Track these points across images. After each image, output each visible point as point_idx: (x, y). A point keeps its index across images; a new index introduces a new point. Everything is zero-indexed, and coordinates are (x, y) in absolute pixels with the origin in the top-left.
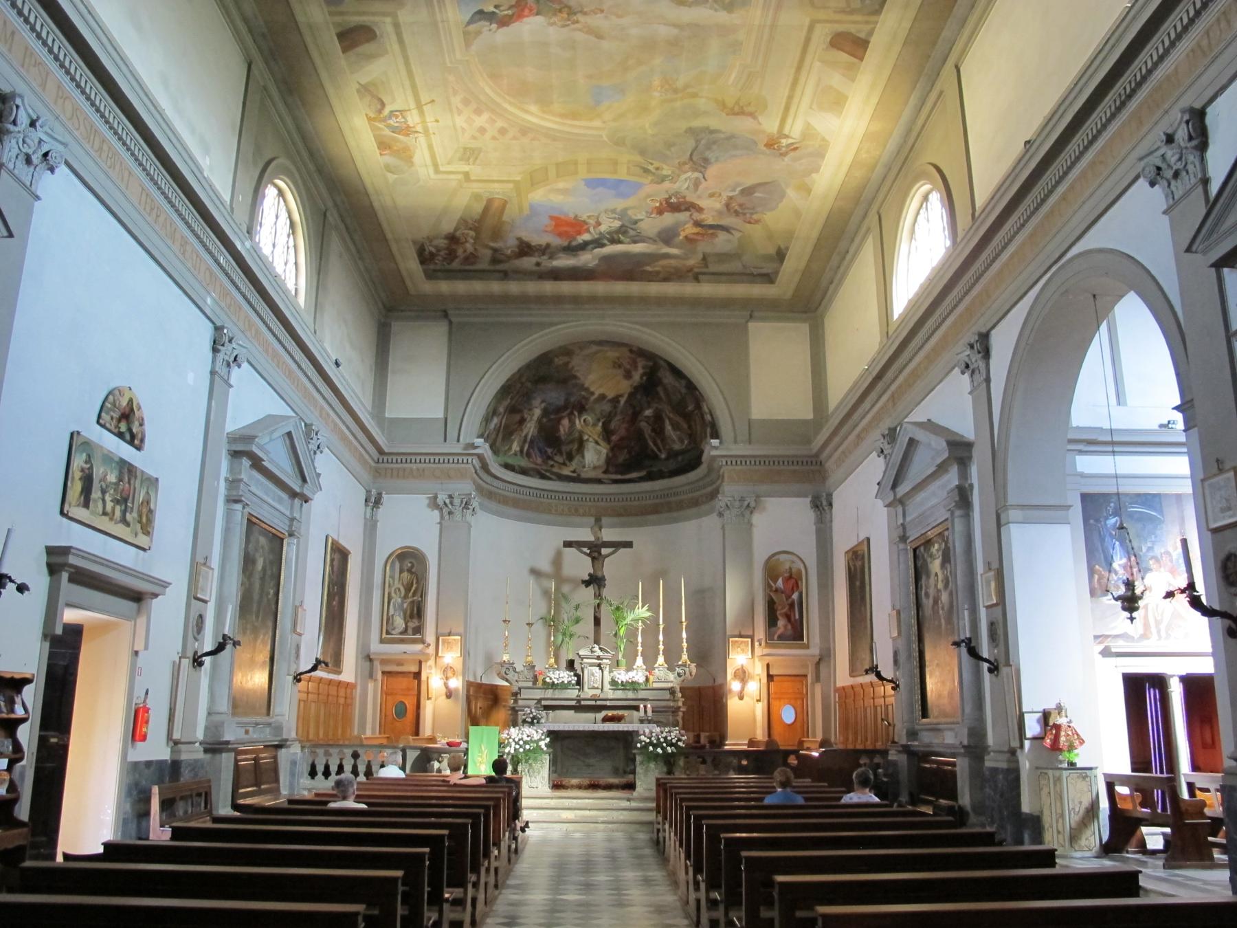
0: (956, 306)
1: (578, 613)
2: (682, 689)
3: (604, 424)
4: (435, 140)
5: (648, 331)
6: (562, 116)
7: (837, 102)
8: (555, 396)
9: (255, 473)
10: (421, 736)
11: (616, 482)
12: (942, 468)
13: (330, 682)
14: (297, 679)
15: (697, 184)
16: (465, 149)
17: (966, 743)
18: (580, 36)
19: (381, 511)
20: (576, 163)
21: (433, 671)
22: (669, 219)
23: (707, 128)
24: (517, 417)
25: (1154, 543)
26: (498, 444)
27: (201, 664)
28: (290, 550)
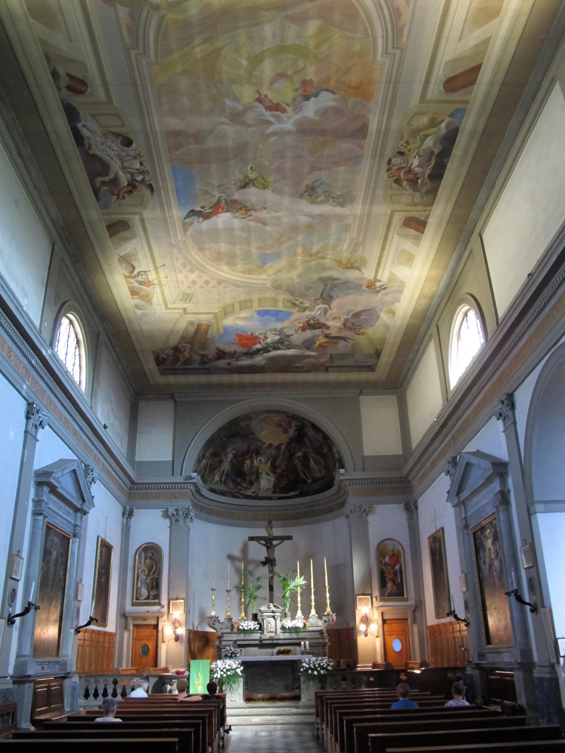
0: (491, 378)
1: (259, 583)
2: (328, 631)
3: (271, 462)
4: (166, 289)
6: (243, 272)
7: (409, 259)
8: (241, 445)
10: (158, 668)
11: (280, 498)
12: (489, 480)
13: (99, 632)
14: (78, 631)
15: (325, 311)
16: (184, 294)
17: (519, 661)
18: (252, 224)
19: (133, 520)
20: (251, 301)
21: (166, 623)
22: (309, 334)
23: (331, 277)
24: (217, 459)
26: (206, 476)
28: (74, 546)
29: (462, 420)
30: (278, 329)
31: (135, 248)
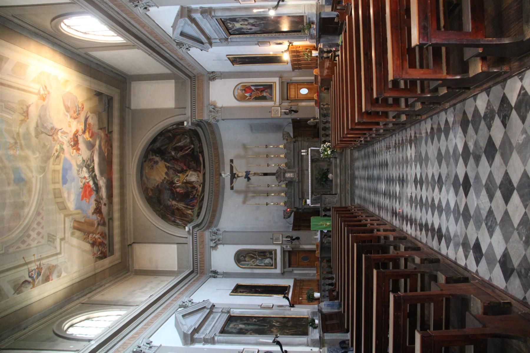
8: (166, 195)
15: (64, 133)
16: (49, 241)
19: (219, 270)
24: (176, 211)
26: (186, 219)
28: (236, 312)
29: (150, 36)
30: (78, 169)
31: (8, 282)
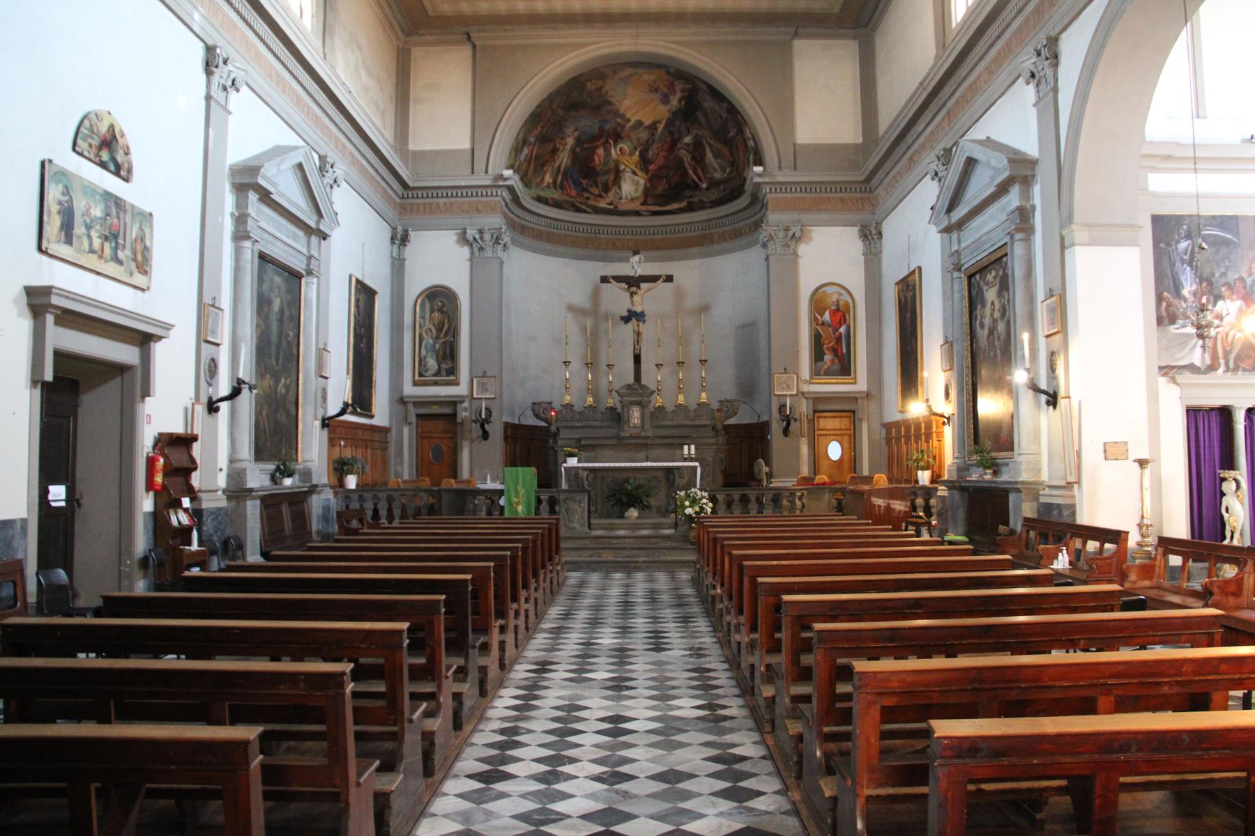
5: (687, 50)
8: (589, 124)
9: (266, 209)
12: (1002, 189)
19: (409, 250)
24: (550, 147)
25: (1227, 268)
27: (217, 410)
28: (309, 289)
